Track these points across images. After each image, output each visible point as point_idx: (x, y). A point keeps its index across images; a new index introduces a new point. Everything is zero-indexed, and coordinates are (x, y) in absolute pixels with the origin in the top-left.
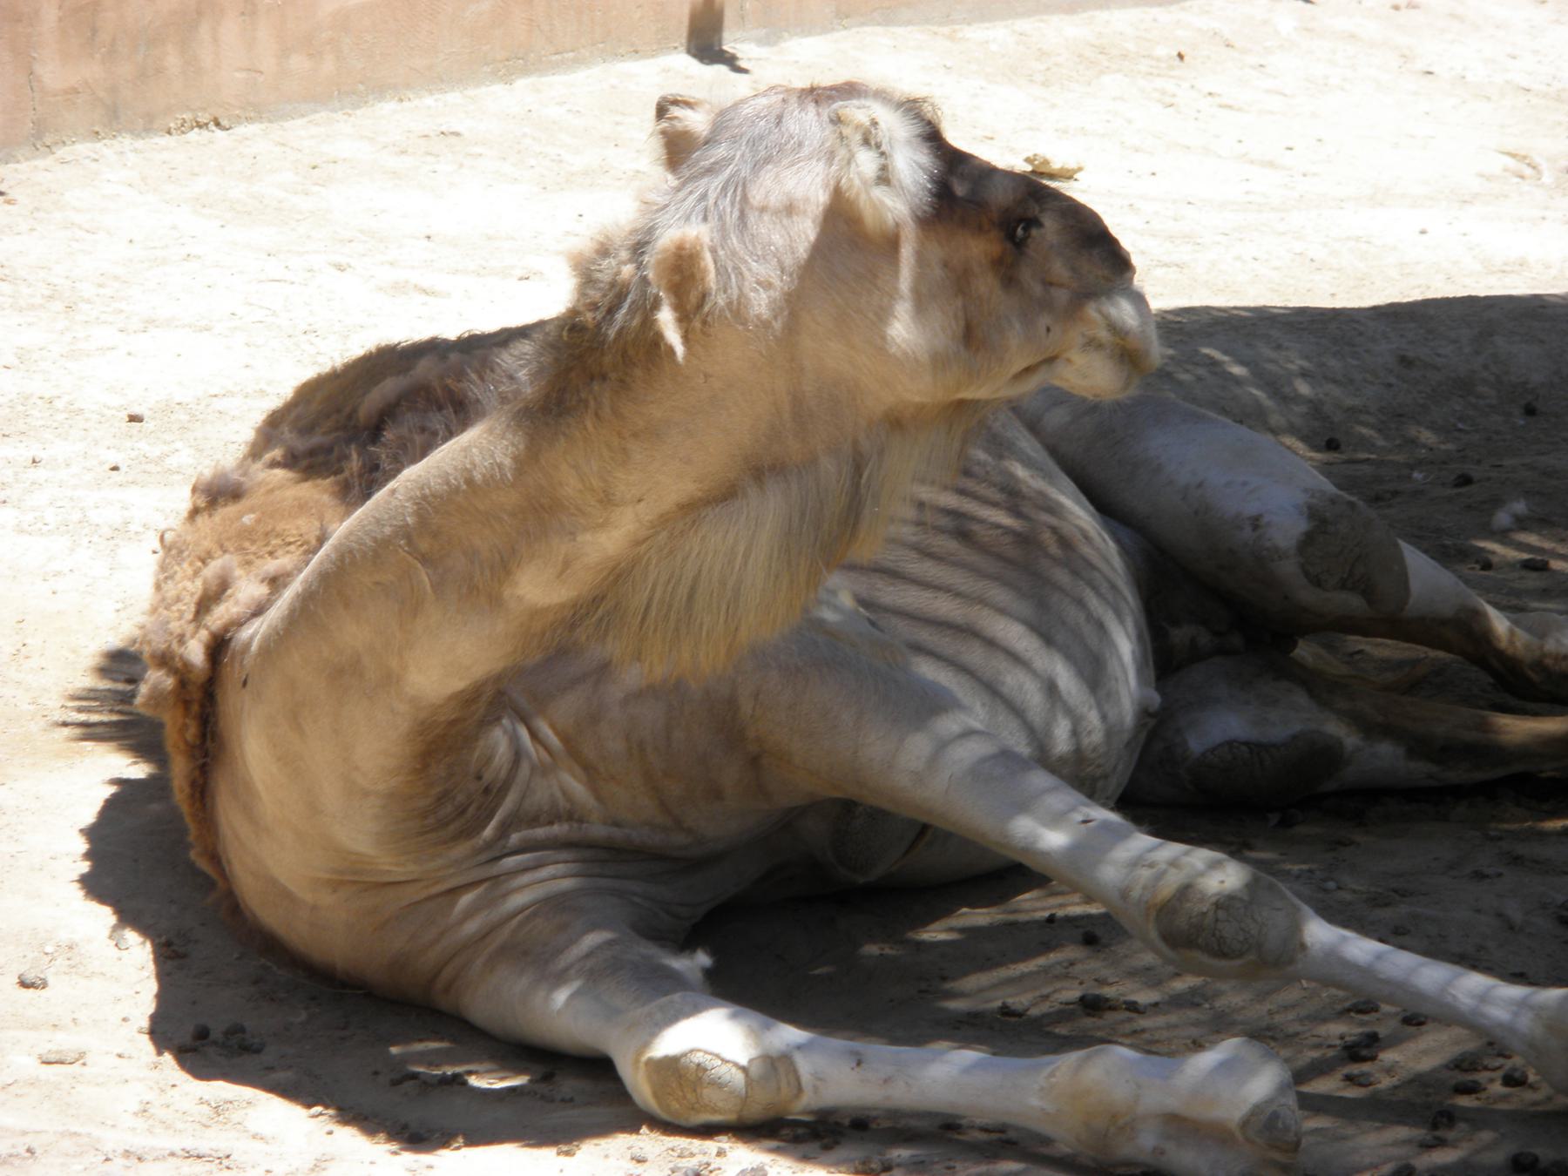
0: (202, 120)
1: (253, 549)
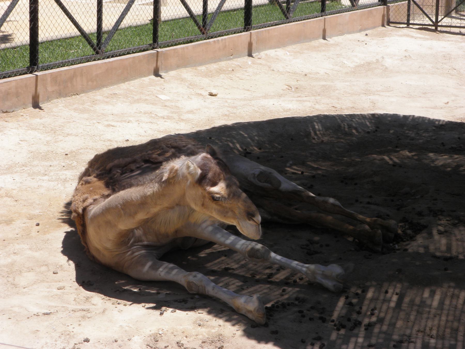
0: (75, 94)
1: (92, 194)
